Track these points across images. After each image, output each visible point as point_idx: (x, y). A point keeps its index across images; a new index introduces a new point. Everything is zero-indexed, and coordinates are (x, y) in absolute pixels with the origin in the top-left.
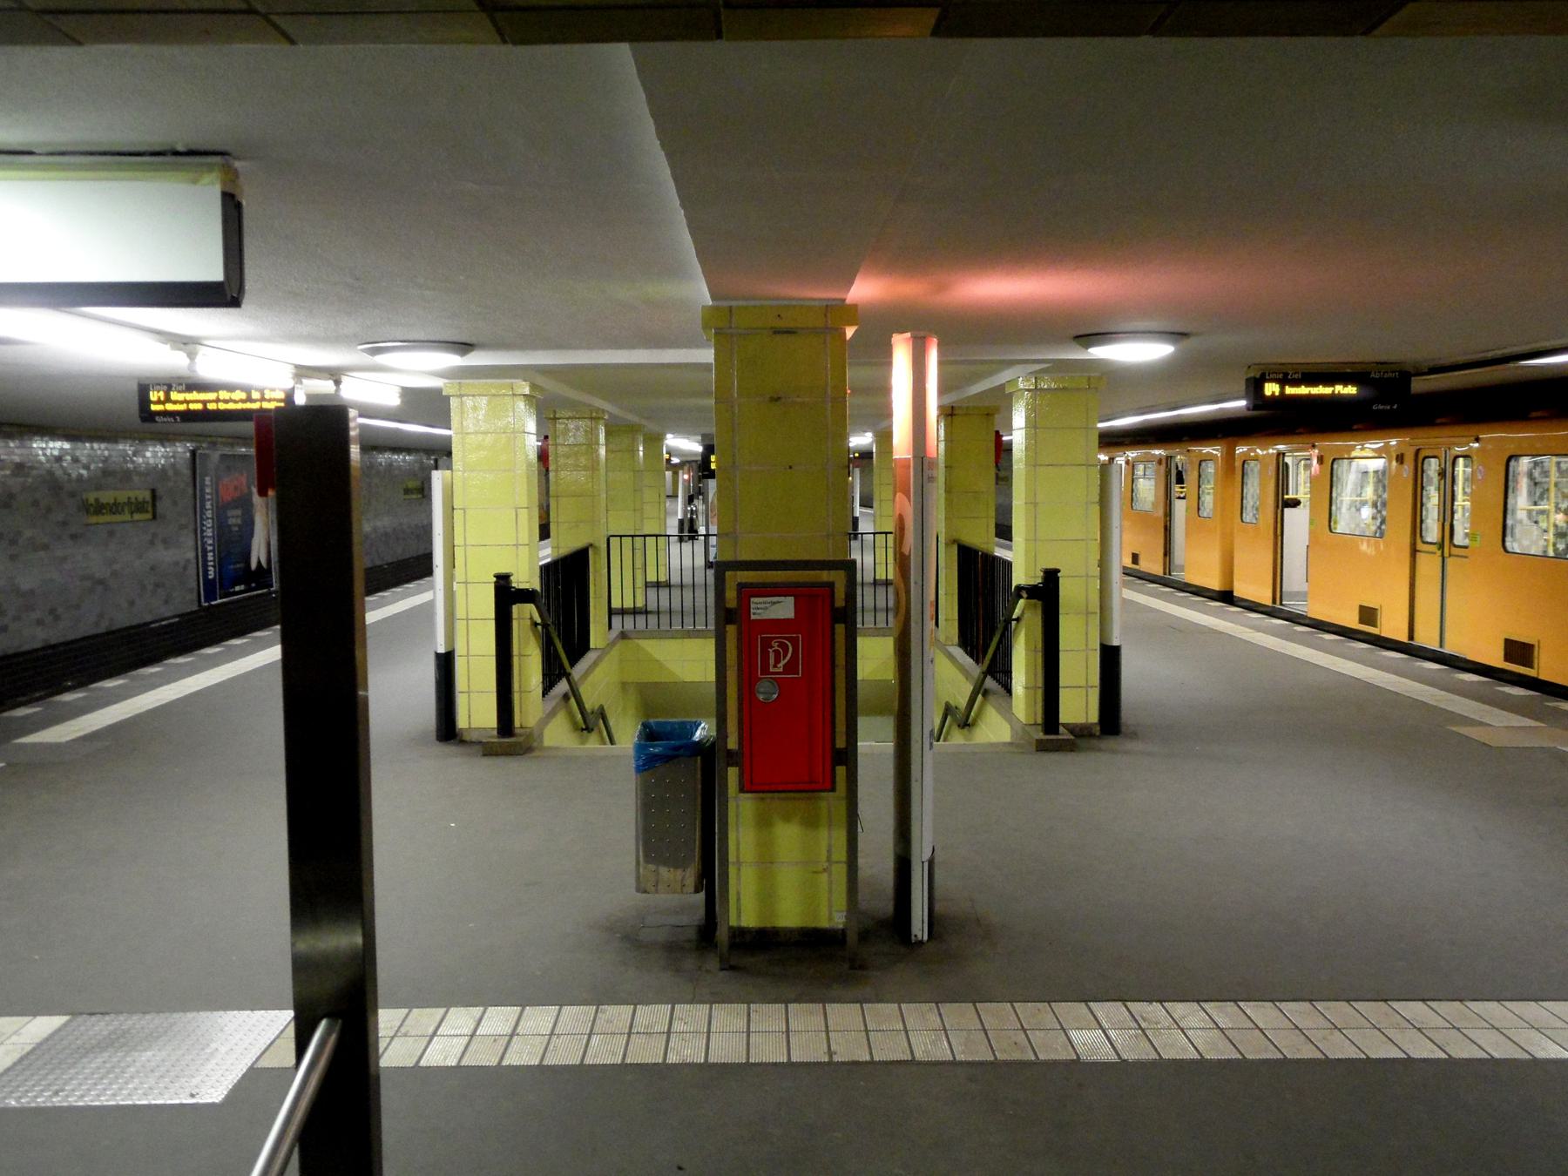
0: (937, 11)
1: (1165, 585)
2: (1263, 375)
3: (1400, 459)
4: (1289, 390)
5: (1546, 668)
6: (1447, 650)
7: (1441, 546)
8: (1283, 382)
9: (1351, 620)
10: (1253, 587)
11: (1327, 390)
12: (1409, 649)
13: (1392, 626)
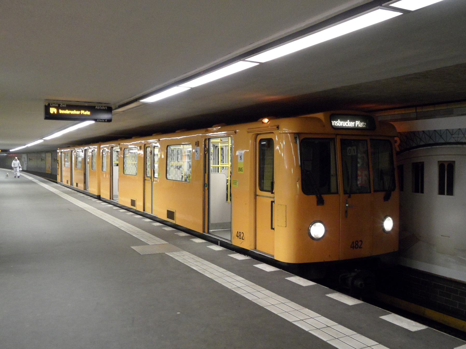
0: (322, 195)
1: (84, 194)
2: (49, 104)
3: (197, 144)
4: (61, 112)
5: (178, 221)
6: (154, 214)
7: (151, 178)
8: (58, 107)
9: (129, 205)
10: (105, 195)
11: (78, 112)
12: (144, 215)
13: (139, 207)
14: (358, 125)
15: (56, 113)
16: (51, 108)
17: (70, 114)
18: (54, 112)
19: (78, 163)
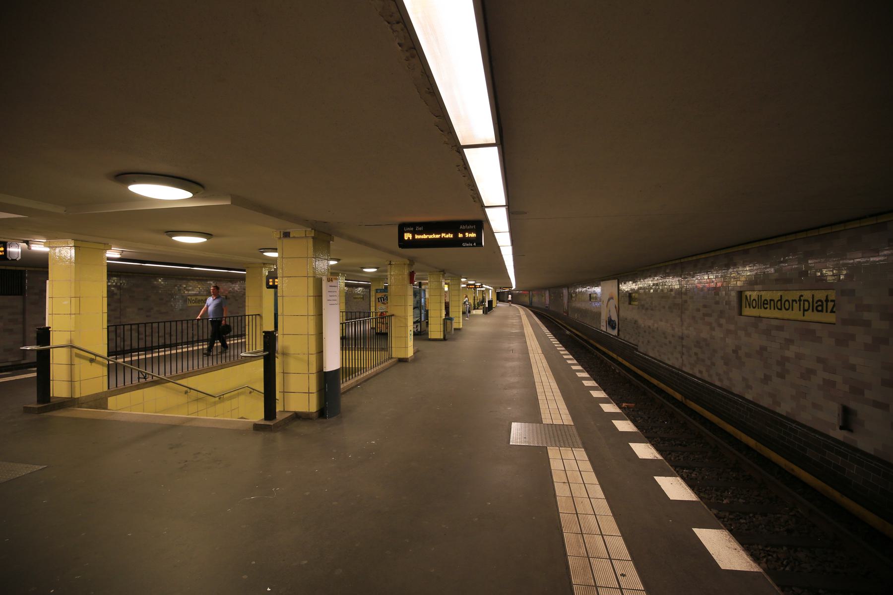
11: (438, 236)
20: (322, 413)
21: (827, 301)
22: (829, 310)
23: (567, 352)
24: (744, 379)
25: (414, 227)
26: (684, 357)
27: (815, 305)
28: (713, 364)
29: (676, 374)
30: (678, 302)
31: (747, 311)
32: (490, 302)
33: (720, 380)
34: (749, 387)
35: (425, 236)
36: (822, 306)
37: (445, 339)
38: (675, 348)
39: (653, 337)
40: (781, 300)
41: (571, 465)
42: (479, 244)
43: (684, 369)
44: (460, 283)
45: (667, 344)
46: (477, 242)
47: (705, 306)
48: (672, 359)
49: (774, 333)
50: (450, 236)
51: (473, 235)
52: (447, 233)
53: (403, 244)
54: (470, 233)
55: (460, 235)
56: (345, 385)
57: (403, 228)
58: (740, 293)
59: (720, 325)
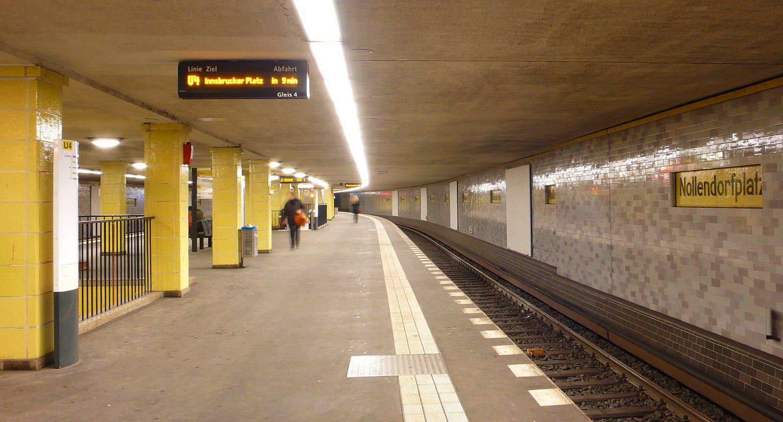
4: (208, 81)
11: (240, 81)
14: (249, 82)
15: (198, 84)
16: (189, 77)
17: (224, 87)
18: (195, 83)
19: (738, 204)
20: (50, 360)
21: (756, 179)
22: (758, 192)
23: (462, 294)
24: (681, 296)
25: (204, 67)
26: (615, 275)
27: (747, 186)
28: (647, 280)
29: (605, 302)
30: (612, 197)
31: (684, 200)
32: (323, 209)
33: (656, 302)
34: (685, 305)
35: (219, 81)
36: (752, 186)
37: (241, 266)
38: (603, 263)
39: (576, 251)
40: (714, 182)
41: (428, 392)
42: (302, 95)
43: (615, 293)
44: (266, 170)
45: (595, 259)
46: (299, 91)
47: (636, 197)
48: (600, 281)
49: (708, 225)
50: (259, 81)
51: (293, 81)
52: (254, 77)
53: (187, 93)
54: (288, 77)
55: (274, 81)
56: (85, 323)
57: (185, 68)
58: (675, 176)
59: (654, 224)
